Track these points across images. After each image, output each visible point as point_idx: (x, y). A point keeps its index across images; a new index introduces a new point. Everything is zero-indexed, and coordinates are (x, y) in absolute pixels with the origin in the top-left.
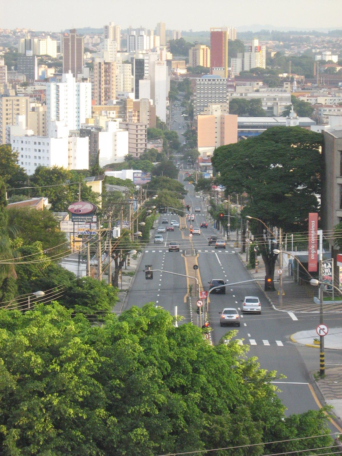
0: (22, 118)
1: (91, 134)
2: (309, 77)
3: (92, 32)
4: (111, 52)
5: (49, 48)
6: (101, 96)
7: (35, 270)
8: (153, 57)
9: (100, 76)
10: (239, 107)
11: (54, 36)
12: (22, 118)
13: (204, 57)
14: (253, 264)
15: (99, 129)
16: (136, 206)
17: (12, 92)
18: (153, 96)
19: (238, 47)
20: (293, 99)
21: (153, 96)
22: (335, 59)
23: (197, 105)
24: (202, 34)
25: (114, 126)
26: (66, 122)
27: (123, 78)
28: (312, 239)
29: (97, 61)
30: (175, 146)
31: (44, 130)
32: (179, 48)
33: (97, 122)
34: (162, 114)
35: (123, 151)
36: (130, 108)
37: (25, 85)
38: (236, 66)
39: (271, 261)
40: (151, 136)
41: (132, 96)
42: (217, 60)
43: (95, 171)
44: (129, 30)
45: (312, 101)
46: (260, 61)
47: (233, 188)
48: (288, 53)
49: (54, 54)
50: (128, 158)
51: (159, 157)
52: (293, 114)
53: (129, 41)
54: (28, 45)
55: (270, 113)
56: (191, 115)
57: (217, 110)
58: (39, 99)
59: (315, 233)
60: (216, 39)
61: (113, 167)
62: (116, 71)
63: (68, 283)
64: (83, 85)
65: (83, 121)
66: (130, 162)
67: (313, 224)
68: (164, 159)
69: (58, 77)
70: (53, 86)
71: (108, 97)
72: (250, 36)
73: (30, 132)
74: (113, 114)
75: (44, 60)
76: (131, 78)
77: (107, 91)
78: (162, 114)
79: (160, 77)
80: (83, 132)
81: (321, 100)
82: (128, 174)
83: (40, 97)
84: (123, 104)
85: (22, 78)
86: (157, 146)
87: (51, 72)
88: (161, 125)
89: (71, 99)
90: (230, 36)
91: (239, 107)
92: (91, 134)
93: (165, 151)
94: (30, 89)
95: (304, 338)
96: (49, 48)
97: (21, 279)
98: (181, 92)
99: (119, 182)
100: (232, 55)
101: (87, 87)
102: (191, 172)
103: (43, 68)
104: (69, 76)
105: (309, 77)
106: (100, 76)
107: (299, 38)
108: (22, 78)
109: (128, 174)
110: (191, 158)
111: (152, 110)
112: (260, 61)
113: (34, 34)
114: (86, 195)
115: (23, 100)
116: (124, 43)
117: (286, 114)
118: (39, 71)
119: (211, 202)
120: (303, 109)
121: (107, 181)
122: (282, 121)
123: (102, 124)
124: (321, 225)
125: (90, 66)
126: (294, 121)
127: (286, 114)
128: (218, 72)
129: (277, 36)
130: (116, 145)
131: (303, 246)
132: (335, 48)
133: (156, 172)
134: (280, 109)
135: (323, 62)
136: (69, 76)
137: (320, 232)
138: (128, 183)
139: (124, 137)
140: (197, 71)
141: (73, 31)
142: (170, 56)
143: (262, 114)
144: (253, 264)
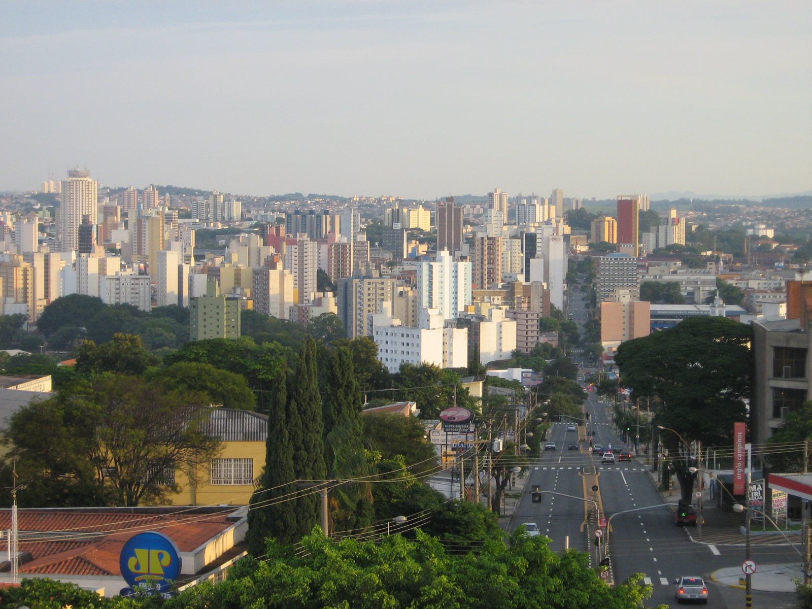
0: (387, 305)
1: (470, 324)
2: (739, 255)
3: (474, 201)
4: (497, 225)
5: (421, 220)
6: (484, 279)
7: (396, 490)
8: (547, 232)
9: (482, 255)
10: (653, 292)
11: (426, 206)
12: (387, 305)
13: (610, 231)
14: (666, 486)
15: (481, 319)
16: (523, 413)
17: (375, 274)
18: (546, 278)
19: (652, 219)
20: (719, 283)
21: (546, 278)
22: (770, 234)
23: (600, 291)
24: (608, 203)
25: (498, 315)
26: (439, 313)
27: (510, 256)
28: (739, 455)
29: (480, 235)
30: (574, 340)
31: (415, 319)
32: (580, 219)
33: (478, 309)
34: (557, 299)
35: (510, 345)
36: (519, 293)
37: (391, 264)
38: (649, 243)
39: (688, 483)
40: (544, 326)
41: (521, 278)
42: (625, 234)
43: (475, 369)
44: (519, 198)
45: (742, 285)
46: (678, 237)
47: (641, 391)
48: (712, 226)
49: (426, 226)
50: (516, 354)
51: (553, 353)
52: (719, 301)
53: (518, 211)
54: (396, 216)
55: (690, 299)
56: (593, 302)
57: (625, 296)
58: (408, 282)
59: (743, 448)
60: (625, 208)
61: (498, 364)
62: (502, 248)
63: (436, 507)
64: (462, 265)
65: (461, 308)
66: (517, 359)
67: (740, 436)
68: (560, 350)
69: (431, 256)
70: (425, 265)
71: (492, 280)
72: (666, 205)
73: (397, 322)
74: (498, 300)
75: (416, 235)
76: (520, 256)
77: (491, 273)
78: (557, 299)
79: (557, 254)
80: (461, 322)
81: (753, 284)
82: (517, 374)
83: (410, 279)
84: (510, 287)
85: (388, 256)
86: (551, 339)
87: (423, 249)
88: (556, 314)
89: (448, 281)
90: (642, 205)
91: (653, 292)
92: (470, 324)
93: (561, 344)
94: (397, 270)
95: (728, 577)
96: (421, 220)
97: (378, 502)
98: (581, 273)
99: (503, 383)
100: (644, 228)
101: (465, 267)
102: (593, 371)
103: (414, 243)
104: (445, 254)
105: (739, 255)
106: (482, 255)
107: (725, 208)
108: (388, 256)
109: (517, 374)
110: (594, 354)
111: (546, 295)
112: (678, 237)
113: (403, 203)
114: (463, 399)
115: (388, 283)
116: (511, 214)
117: (710, 300)
118: (407, 248)
119: (617, 409)
120: (730, 295)
121: (489, 382)
122: (704, 309)
123: (484, 312)
124: (749, 439)
125: (471, 242)
126: (721, 309)
127: (710, 300)
128: (626, 249)
129: (699, 205)
130: (500, 337)
131: (728, 463)
132: (770, 220)
133: (549, 371)
134: (702, 295)
135: (755, 238)
136: (445, 254)
137: (748, 447)
138: (515, 384)
139: (511, 328)
140: (601, 248)
141: (450, 199)
142: (568, 230)
143: (680, 301)
144: (666, 486)
